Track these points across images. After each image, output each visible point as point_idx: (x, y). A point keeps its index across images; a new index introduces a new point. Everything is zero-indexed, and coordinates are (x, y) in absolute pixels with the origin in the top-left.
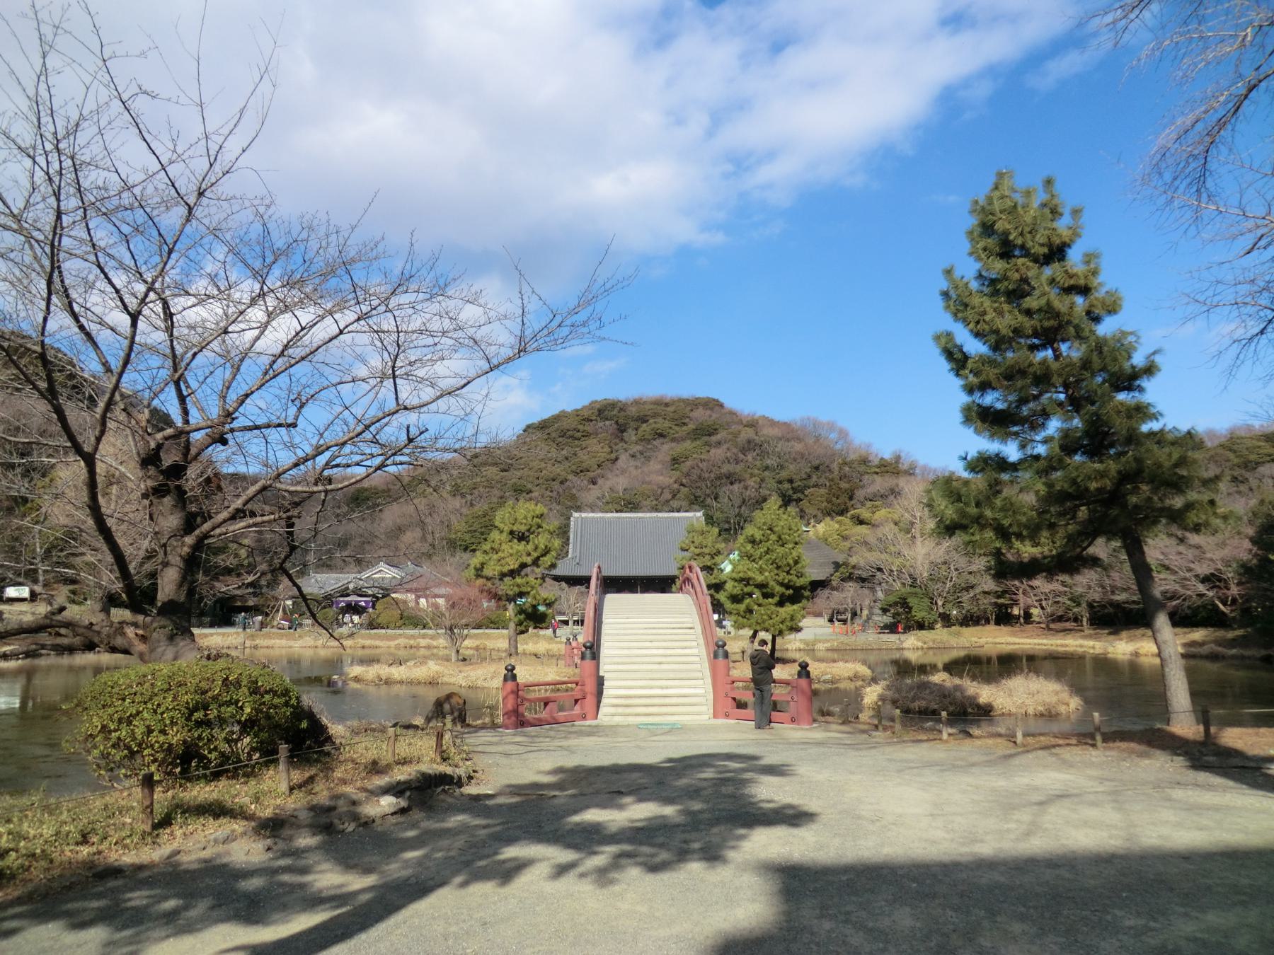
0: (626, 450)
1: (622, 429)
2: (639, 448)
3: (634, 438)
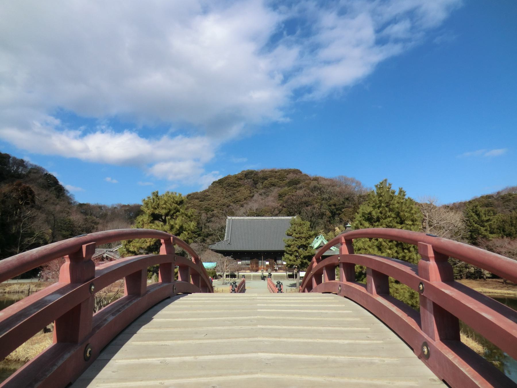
0: (257, 192)
1: (255, 183)
3: (261, 186)
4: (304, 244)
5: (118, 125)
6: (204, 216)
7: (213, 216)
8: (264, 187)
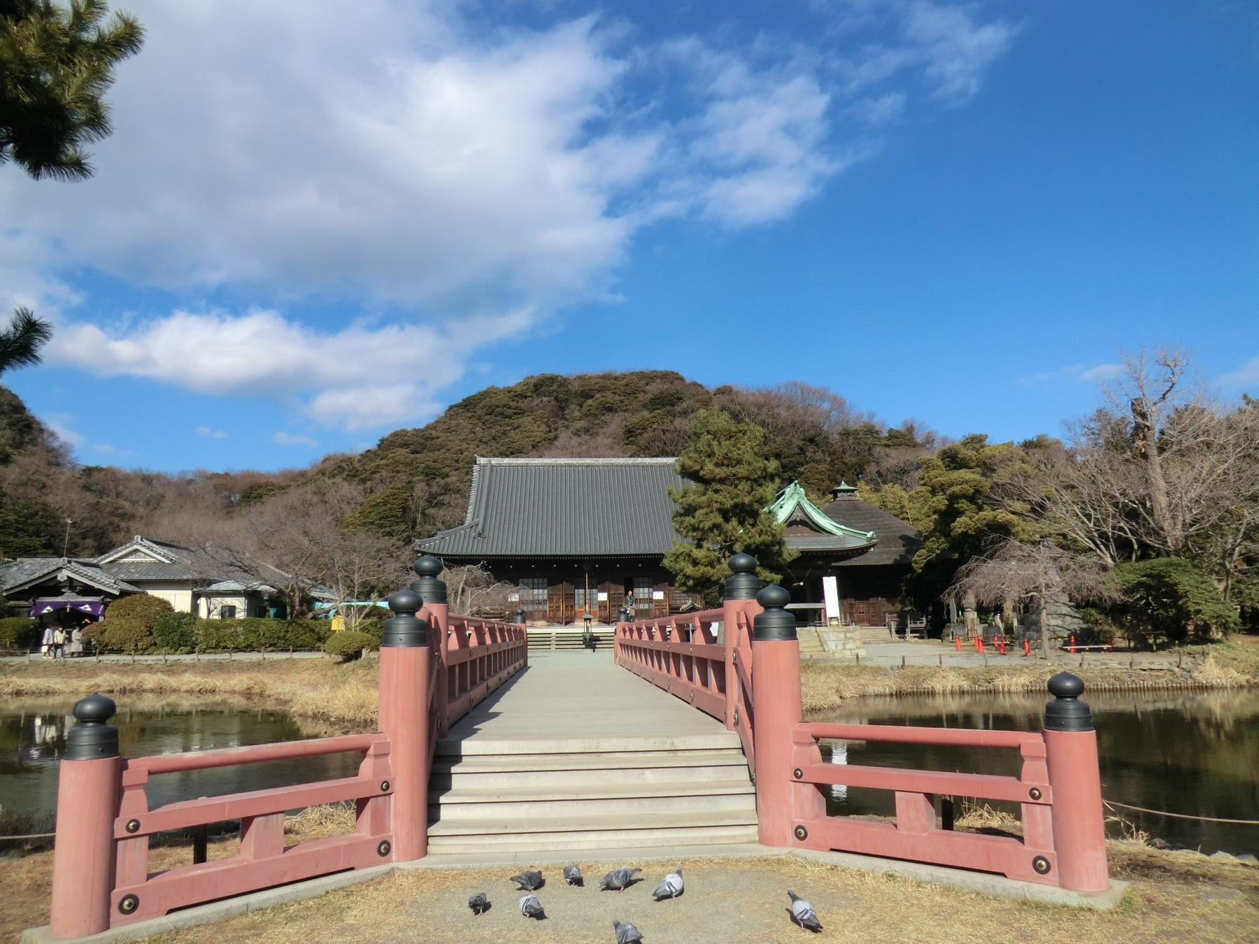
0: (567, 427)
1: (561, 407)
2: (582, 424)
3: (577, 414)
4: (747, 500)
5: (229, 302)
6: (420, 489)
7: (446, 490)
8: (586, 415)
